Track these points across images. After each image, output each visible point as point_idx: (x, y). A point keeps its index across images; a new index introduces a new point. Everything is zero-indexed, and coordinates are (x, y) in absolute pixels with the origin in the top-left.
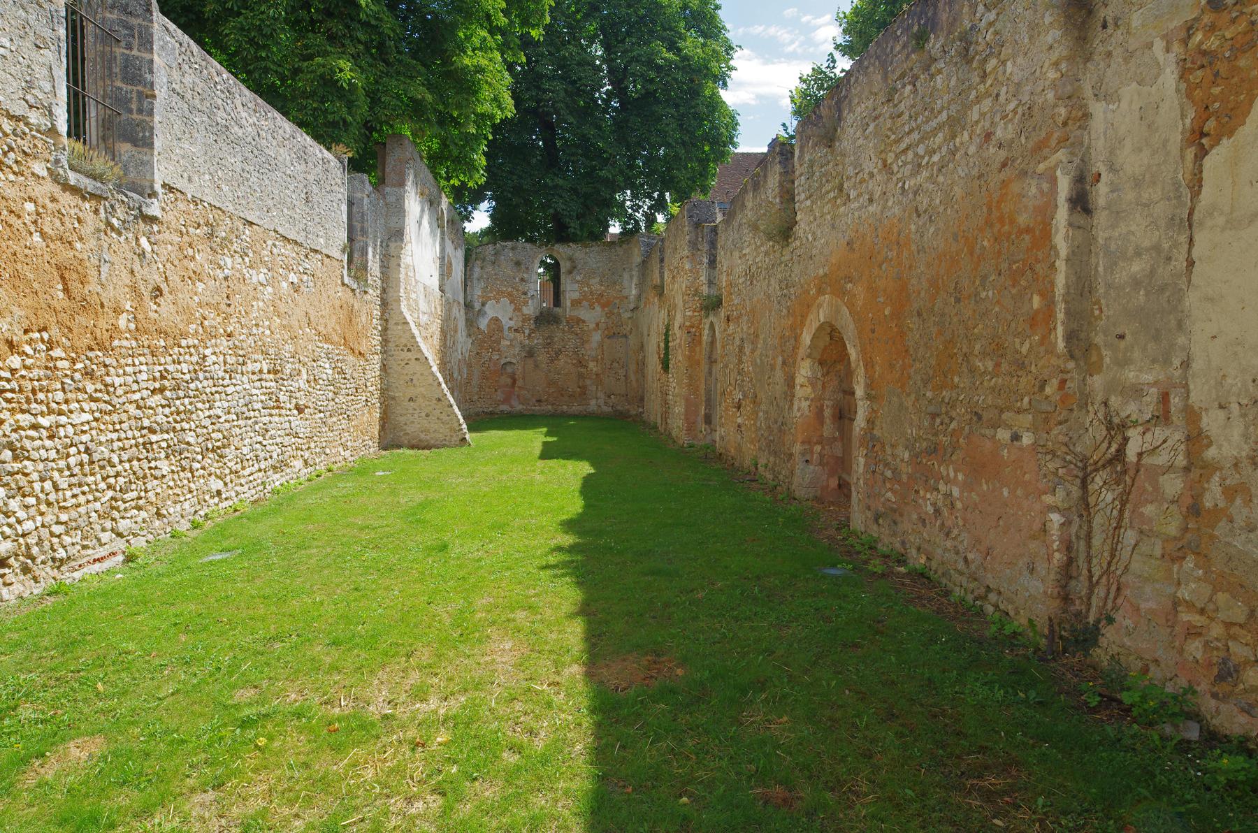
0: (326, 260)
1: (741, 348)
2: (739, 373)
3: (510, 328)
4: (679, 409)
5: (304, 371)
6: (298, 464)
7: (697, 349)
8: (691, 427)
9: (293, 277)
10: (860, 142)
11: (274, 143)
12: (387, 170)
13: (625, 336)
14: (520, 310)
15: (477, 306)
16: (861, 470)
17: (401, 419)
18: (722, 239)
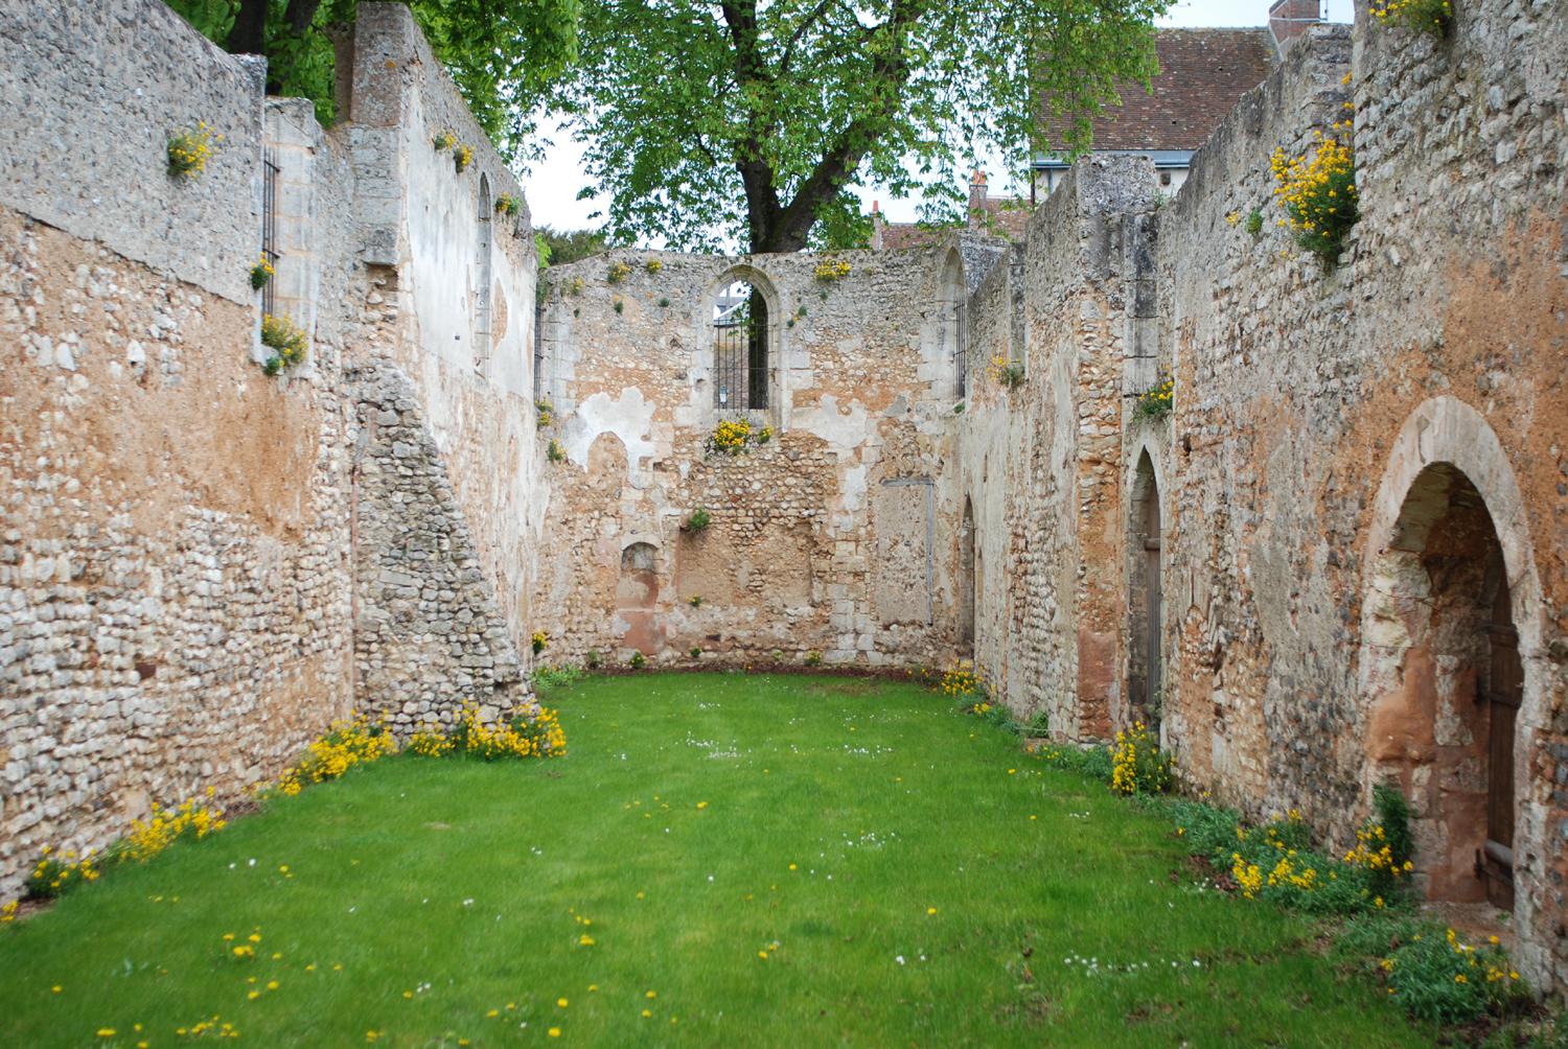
0: (214, 308)
2: (1215, 580)
3: (644, 461)
6: (135, 801)
9: (137, 352)
10: (1523, 26)
11: (101, 33)
12: (357, 87)
13: (926, 479)
14: (669, 417)
16: (1538, 836)
17: (511, 516)
18: (1170, 247)
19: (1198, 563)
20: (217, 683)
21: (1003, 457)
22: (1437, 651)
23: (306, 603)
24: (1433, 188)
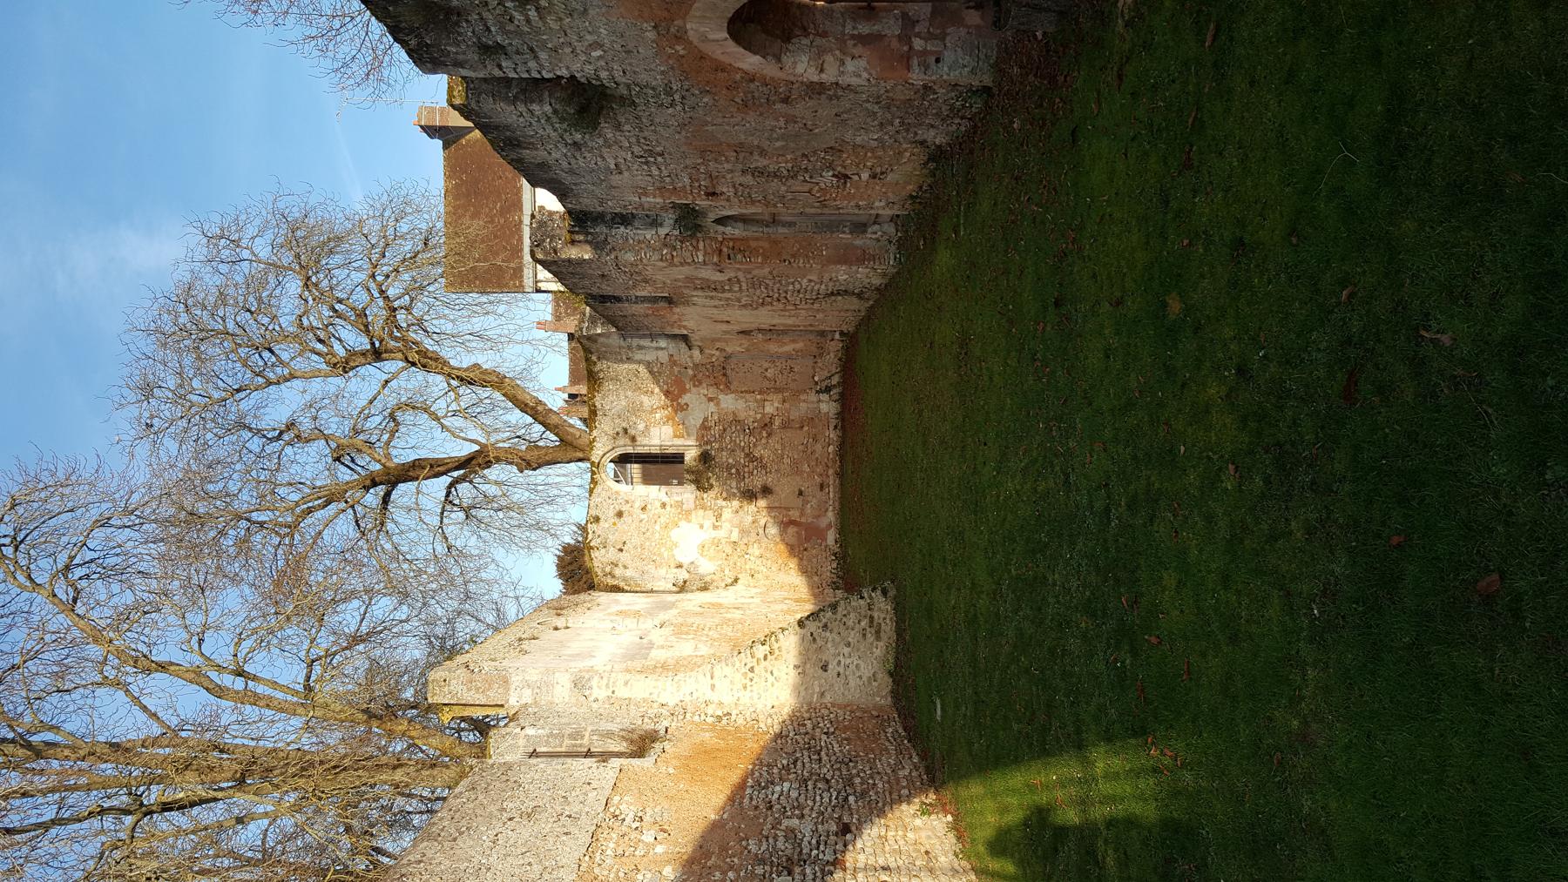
1: (759, 173)
3: (715, 527)
4: (840, 274)
5: (786, 823)
7: (753, 244)
8: (863, 258)
13: (727, 358)
15: (683, 575)
18: (588, 203)
19: (784, 188)
20: (852, 785)
21: (715, 311)
22: (843, 34)
23: (803, 730)
24: (555, 26)
